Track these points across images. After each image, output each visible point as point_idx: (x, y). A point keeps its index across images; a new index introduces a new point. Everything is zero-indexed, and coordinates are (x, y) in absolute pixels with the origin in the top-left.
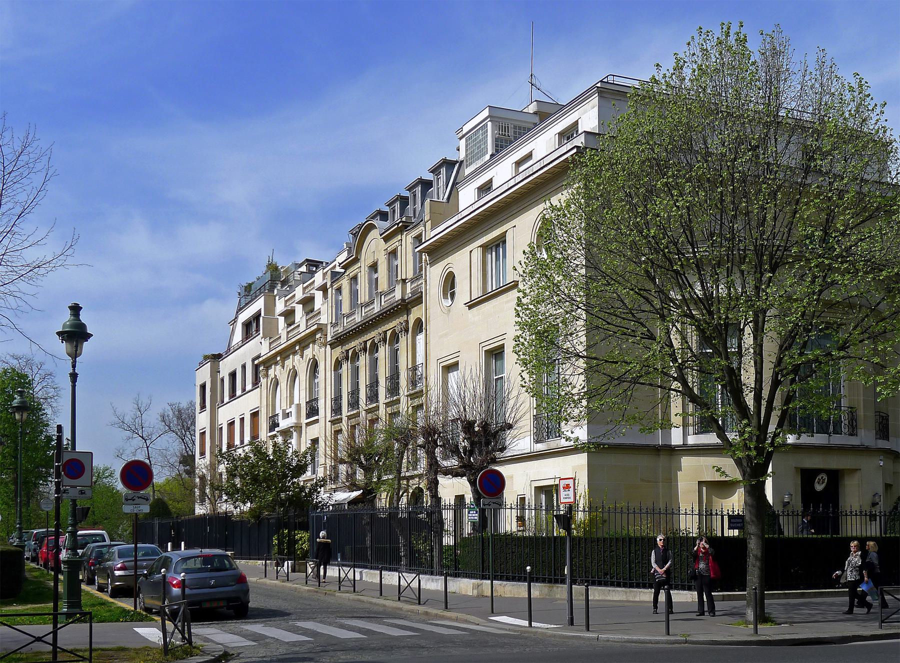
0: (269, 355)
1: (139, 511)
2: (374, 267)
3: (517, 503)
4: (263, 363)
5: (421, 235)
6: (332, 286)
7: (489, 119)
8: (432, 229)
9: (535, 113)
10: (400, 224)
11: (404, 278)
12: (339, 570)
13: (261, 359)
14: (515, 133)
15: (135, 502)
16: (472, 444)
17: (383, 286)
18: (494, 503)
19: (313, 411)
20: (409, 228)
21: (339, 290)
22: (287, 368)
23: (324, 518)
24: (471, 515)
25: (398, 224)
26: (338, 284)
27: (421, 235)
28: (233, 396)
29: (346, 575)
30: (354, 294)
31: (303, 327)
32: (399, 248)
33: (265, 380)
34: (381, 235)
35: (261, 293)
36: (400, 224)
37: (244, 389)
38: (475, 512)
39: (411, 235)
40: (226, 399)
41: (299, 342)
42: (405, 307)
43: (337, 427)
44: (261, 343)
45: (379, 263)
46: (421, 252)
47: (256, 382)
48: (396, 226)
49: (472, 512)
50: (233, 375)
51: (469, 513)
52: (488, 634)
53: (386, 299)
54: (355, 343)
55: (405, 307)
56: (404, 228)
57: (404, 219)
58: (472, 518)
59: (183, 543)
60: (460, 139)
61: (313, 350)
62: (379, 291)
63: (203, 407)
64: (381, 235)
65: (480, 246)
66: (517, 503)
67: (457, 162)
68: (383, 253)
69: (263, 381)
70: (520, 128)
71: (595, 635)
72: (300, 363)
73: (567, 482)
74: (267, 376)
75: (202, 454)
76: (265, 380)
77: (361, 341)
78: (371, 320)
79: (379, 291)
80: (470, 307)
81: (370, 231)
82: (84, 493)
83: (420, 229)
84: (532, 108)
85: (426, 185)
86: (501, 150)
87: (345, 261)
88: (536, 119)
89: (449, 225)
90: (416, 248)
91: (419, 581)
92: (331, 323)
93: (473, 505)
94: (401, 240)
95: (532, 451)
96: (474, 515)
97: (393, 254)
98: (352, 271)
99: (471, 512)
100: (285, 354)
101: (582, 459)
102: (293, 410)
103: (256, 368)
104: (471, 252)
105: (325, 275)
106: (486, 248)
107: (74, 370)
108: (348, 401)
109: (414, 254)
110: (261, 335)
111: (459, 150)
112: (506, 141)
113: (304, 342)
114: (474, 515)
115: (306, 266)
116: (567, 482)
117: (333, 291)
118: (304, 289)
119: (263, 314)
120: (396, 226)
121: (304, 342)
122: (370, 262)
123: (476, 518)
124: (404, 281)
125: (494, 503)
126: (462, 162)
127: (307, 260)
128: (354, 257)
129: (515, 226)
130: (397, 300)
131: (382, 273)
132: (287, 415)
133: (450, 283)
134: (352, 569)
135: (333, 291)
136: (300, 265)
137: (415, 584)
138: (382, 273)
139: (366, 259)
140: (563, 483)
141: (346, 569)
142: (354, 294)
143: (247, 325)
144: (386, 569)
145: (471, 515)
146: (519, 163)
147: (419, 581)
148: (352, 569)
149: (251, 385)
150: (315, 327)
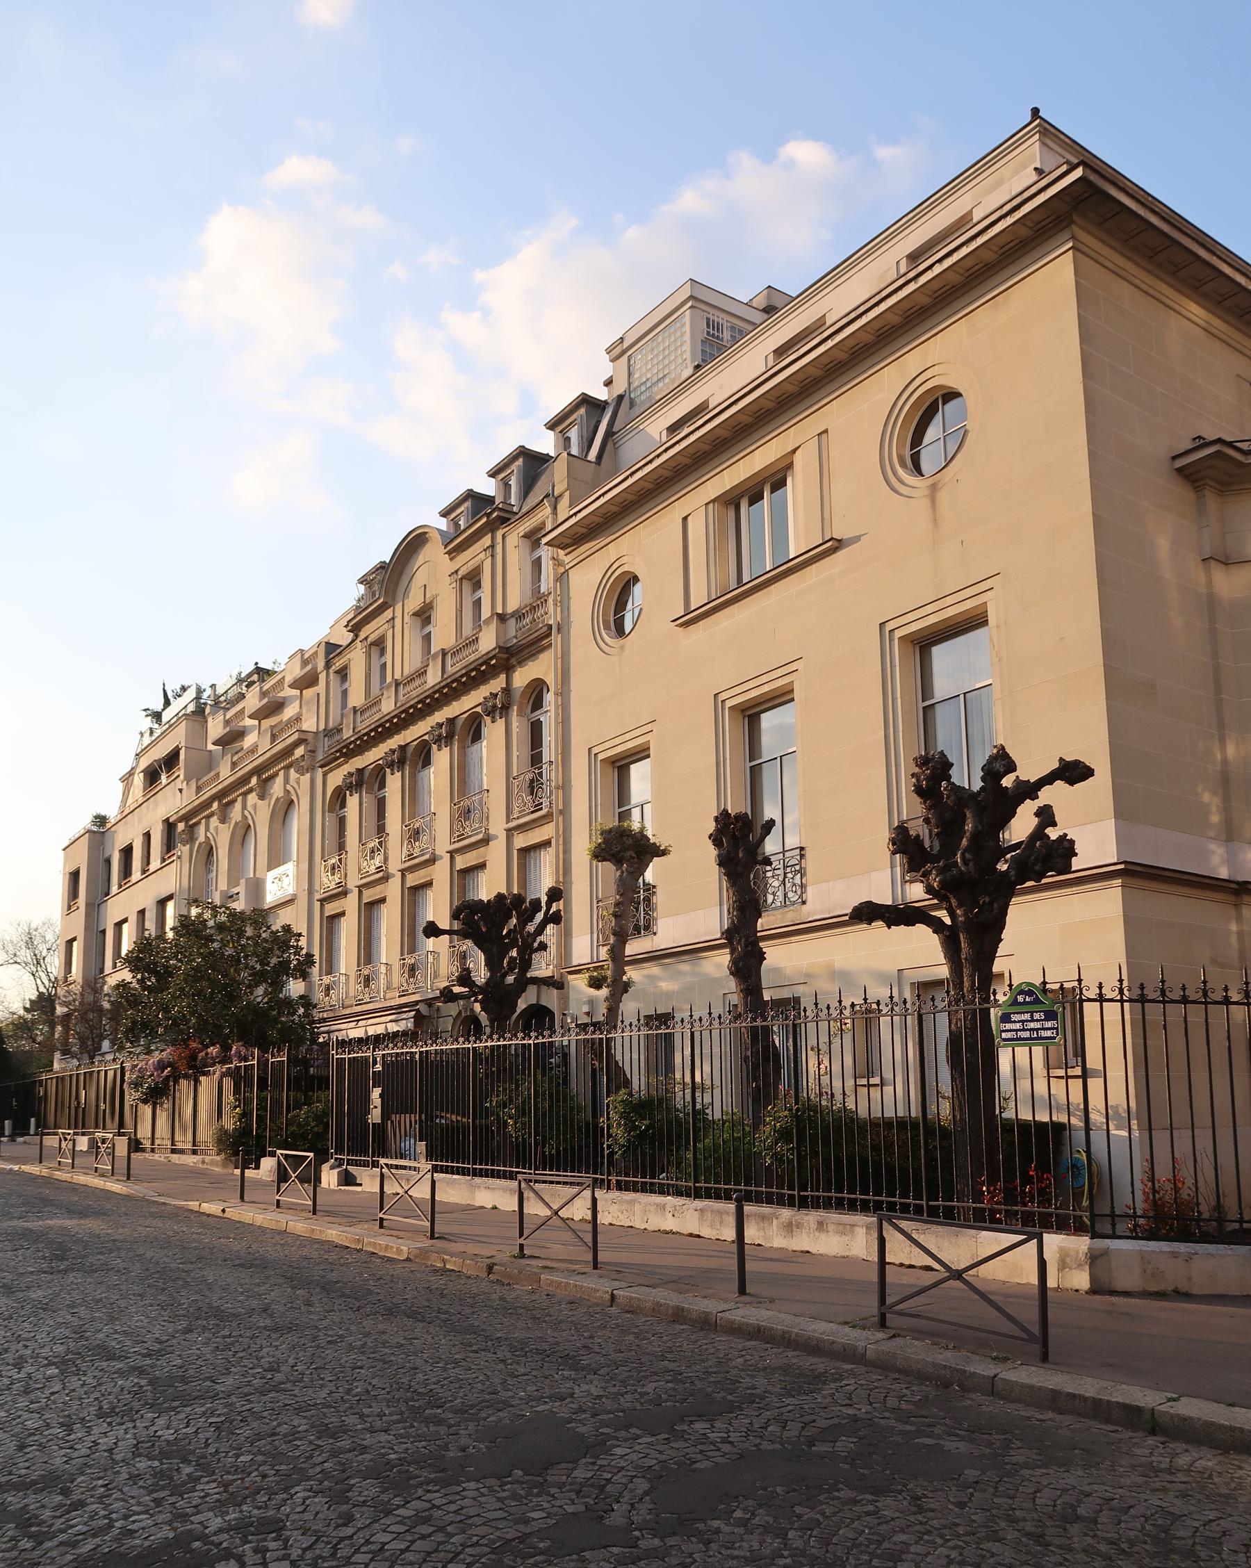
3: (1121, 981)
4: (185, 818)
6: (328, 665)
7: (690, 304)
10: (495, 515)
32: (487, 565)
34: (446, 546)
36: (495, 515)
39: (517, 532)
40: (114, 889)
41: (257, 771)
48: (485, 520)
53: (751, 328)
54: (375, 755)
56: (499, 523)
64: (446, 546)
65: (713, 501)
66: (1121, 981)
72: (259, 810)
77: (395, 747)
80: (686, 624)
83: (367, 723)
89: (614, 488)
104: (685, 519)
106: (731, 501)
113: (263, 774)
117: (332, 675)
118: (234, 764)
120: (485, 520)
121: (263, 774)
122: (414, 601)
128: (382, 600)
129: (826, 431)
134: (587, 1193)
144: (758, 1199)
148: (587, 1193)
150: (296, 736)
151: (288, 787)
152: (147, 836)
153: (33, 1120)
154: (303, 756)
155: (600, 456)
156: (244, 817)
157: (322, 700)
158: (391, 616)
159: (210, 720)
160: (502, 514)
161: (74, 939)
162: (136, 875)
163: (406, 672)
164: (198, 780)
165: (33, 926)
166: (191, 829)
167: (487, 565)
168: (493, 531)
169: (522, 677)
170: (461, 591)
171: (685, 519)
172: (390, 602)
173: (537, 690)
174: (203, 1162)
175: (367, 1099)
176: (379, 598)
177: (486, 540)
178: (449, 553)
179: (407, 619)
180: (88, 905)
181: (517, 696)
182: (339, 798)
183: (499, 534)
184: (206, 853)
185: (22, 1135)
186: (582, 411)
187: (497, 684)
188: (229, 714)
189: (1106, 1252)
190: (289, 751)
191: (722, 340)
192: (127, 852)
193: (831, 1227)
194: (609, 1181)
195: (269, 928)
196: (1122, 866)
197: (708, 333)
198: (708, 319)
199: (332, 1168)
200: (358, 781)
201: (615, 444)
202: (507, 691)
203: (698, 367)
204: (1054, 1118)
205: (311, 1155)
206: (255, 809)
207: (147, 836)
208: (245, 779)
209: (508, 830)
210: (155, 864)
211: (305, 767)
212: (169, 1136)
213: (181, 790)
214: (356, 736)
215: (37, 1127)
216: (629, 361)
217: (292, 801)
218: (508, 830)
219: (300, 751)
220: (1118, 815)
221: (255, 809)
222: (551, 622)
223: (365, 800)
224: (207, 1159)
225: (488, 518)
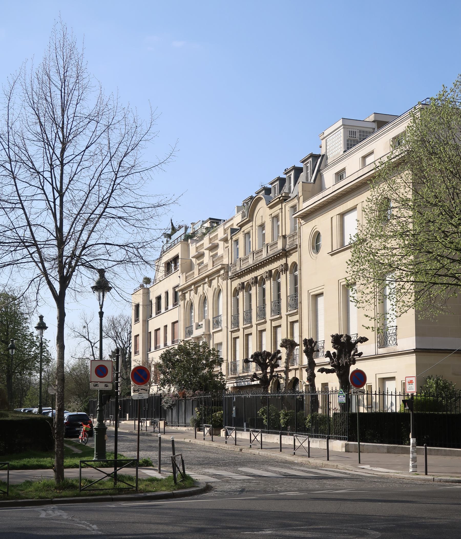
0: (186, 285)
1: (142, 397)
2: (262, 226)
4: (182, 290)
5: (295, 205)
6: (231, 238)
8: (304, 201)
9: (374, 122)
10: (281, 198)
11: (284, 234)
12: (250, 434)
13: (180, 288)
14: (360, 135)
15: (139, 392)
16: (340, 351)
17: (268, 240)
18: (360, 392)
19: (217, 323)
20: (287, 201)
21: (237, 241)
22: (199, 294)
23: (234, 399)
24: (340, 398)
25: (279, 198)
26: (236, 237)
27: (295, 205)
28: (159, 313)
29: (256, 437)
30: (247, 244)
31: (210, 267)
32: (280, 214)
33: (183, 302)
34: (267, 205)
35: (178, 243)
36: (281, 198)
37: (167, 308)
38: (343, 396)
40: (154, 315)
42: (285, 253)
43: (235, 335)
44: (179, 277)
45: (266, 224)
46: (295, 217)
47: (176, 303)
48: (278, 199)
49: (341, 396)
50: (159, 298)
51: (339, 397)
52: (362, 476)
54: (248, 278)
55: (285, 253)
56: (283, 200)
57: (283, 195)
58: (341, 400)
59: (127, 414)
60: (322, 139)
61: (218, 282)
62: (266, 243)
63: (137, 320)
64: (267, 205)
65: (339, 214)
67: (320, 155)
68: (269, 217)
69: (181, 303)
70: (363, 132)
71: (431, 477)
72: (209, 291)
73: (411, 379)
74: (184, 298)
75: (136, 352)
76: (183, 302)
78: (261, 263)
79: (266, 243)
80: (332, 255)
81: (259, 202)
82: (108, 386)
84: (372, 118)
85: (298, 171)
86: (351, 148)
87: (241, 222)
88: (374, 125)
90: (293, 215)
91: (309, 442)
92: (231, 264)
93: (341, 391)
94: (282, 208)
95: (377, 354)
96: (342, 398)
97: (276, 218)
98: (246, 228)
99: (340, 396)
100: (196, 284)
101: (412, 359)
102: (203, 322)
103: (176, 294)
104: (332, 218)
105: (225, 230)
107: (101, 310)
108: (244, 318)
109: (291, 219)
110: (180, 271)
111: (321, 147)
112: (354, 141)
113: (210, 278)
114: (342, 398)
115: (210, 223)
116: (411, 379)
117: (233, 242)
119: (180, 257)
120: (278, 199)
121: (210, 278)
122: (259, 222)
123: (344, 400)
124: (284, 237)
125: (360, 392)
126: (323, 155)
127: (210, 219)
128: (248, 219)
130: (279, 249)
131: (268, 230)
132: (199, 326)
133: (317, 237)
135: (233, 242)
136: (206, 222)
137: (306, 445)
138: (268, 230)
139: (257, 220)
140: (408, 380)
141: (256, 434)
142: (247, 244)
143: (168, 265)
144: (266, 432)
145: (340, 398)
146: (364, 158)
147: (309, 442)
148: (260, 434)
149: (172, 305)
150: (220, 267)
151: (219, 284)
152: (167, 293)
153: (127, 414)
154: (224, 274)
155: (315, 180)
156: (204, 293)
157: (230, 251)
158: (251, 225)
159: (190, 245)
160: (284, 198)
161: (138, 335)
162: (163, 310)
163: (257, 249)
164: (186, 273)
165: (115, 317)
166: (184, 295)
167: (280, 214)
168: (282, 203)
169: (290, 260)
170: (273, 222)
171: (332, 218)
172: (251, 220)
173: (295, 265)
174: (188, 429)
175: (232, 410)
176: (247, 218)
177: (280, 206)
178: (269, 207)
179: (257, 228)
180: (143, 321)
181: (289, 265)
182: (236, 293)
183: (284, 204)
184: (190, 305)
185: (124, 420)
186: (311, 159)
187: (283, 261)
188: (198, 245)
189: (348, 444)
190: (218, 271)
191: (355, 137)
192: (159, 298)
193: (314, 441)
194: (312, 435)
195: (208, 348)
196: (413, 351)
197: (350, 137)
198: (350, 131)
199: (223, 430)
200: (242, 286)
201: (321, 174)
202: (286, 264)
203: (345, 151)
204: (137, 422)
205: (211, 425)
206: (208, 290)
207: (167, 293)
208: (203, 279)
209: (287, 315)
210: (170, 306)
211: (226, 278)
212: (177, 421)
213: (179, 277)
214: (240, 271)
215: (129, 417)
216: (326, 141)
217: (221, 289)
218: (287, 315)
219: (222, 272)
220: (417, 334)
221: (208, 290)
222: (297, 243)
223: (244, 295)
224: (189, 428)
225: (279, 199)
